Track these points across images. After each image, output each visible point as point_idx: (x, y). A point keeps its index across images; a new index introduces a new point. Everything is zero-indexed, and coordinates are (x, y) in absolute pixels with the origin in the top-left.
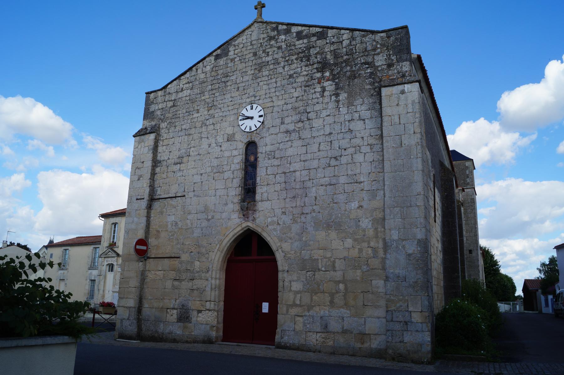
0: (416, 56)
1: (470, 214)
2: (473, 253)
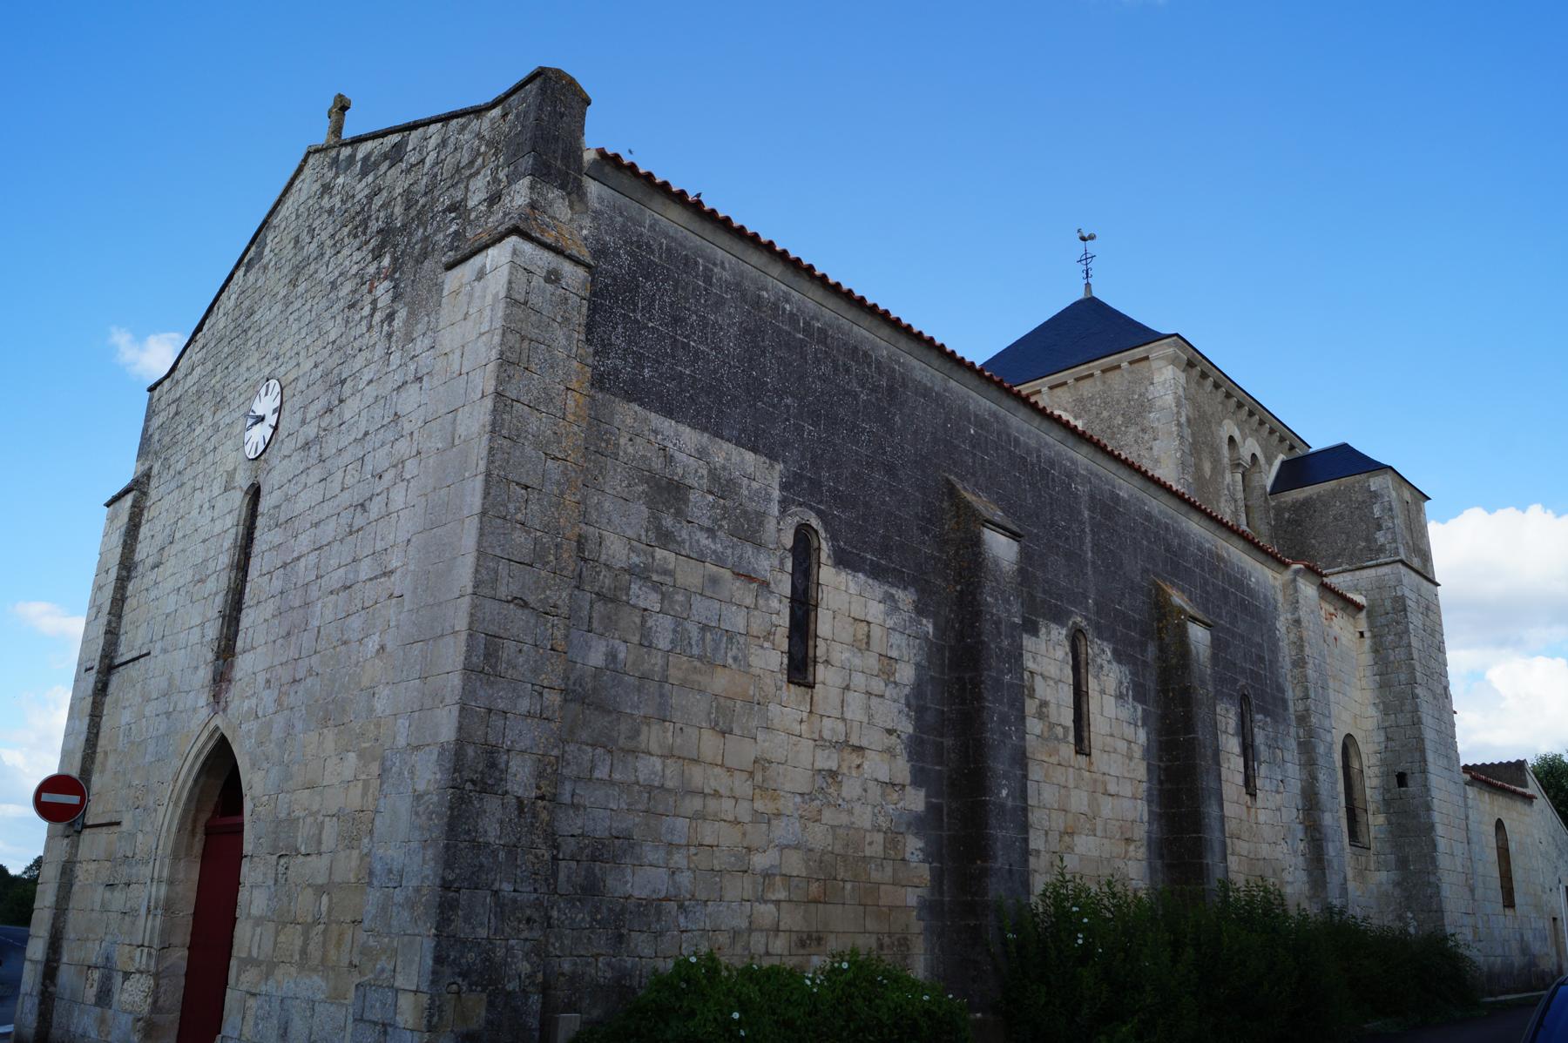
2: (1410, 783)
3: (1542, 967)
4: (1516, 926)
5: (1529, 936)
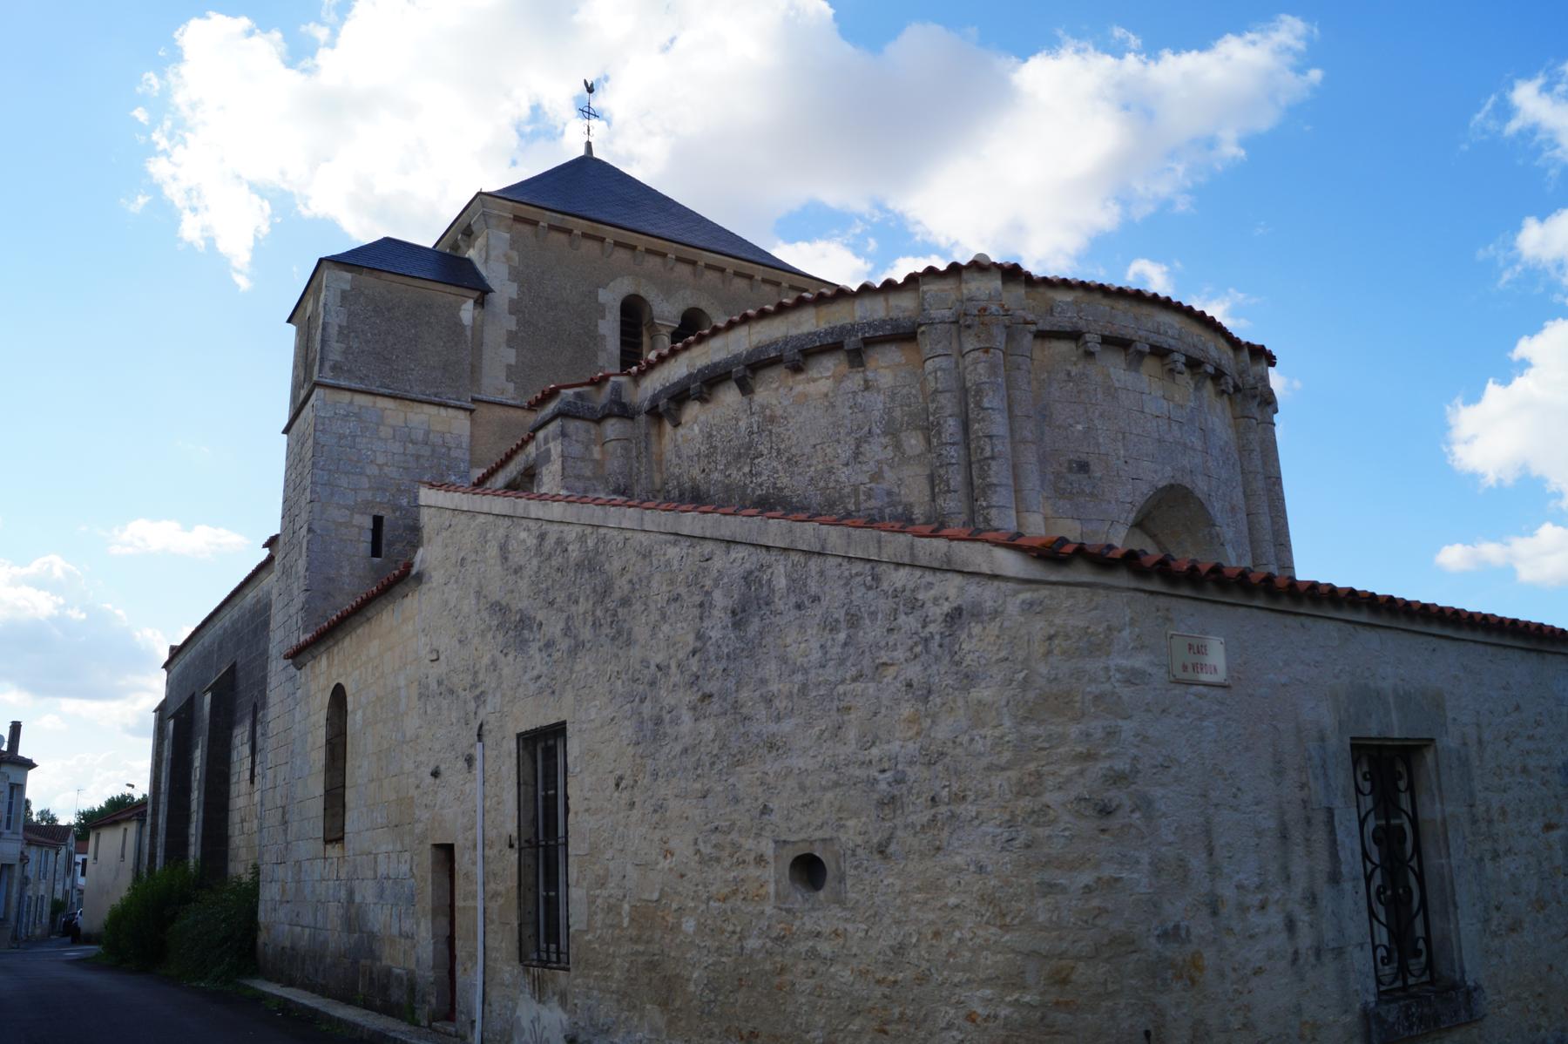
3: (386, 962)
4: (343, 876)
5: (366, 893)
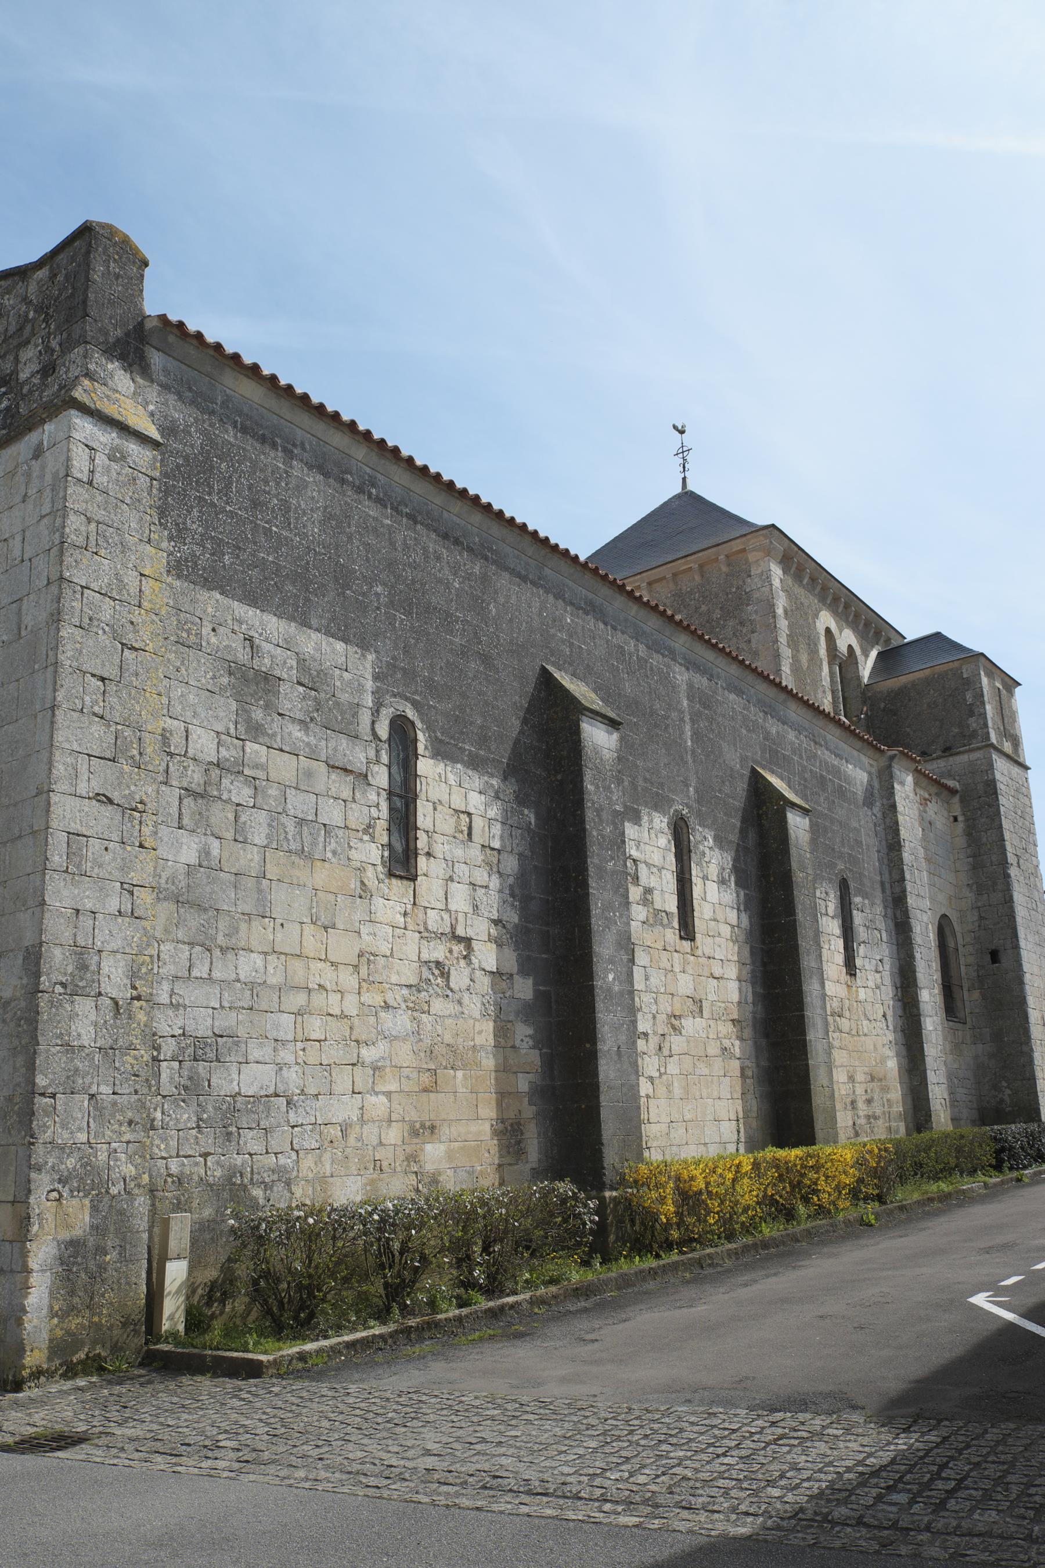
0: (156, 323)
1: (986, 831)
